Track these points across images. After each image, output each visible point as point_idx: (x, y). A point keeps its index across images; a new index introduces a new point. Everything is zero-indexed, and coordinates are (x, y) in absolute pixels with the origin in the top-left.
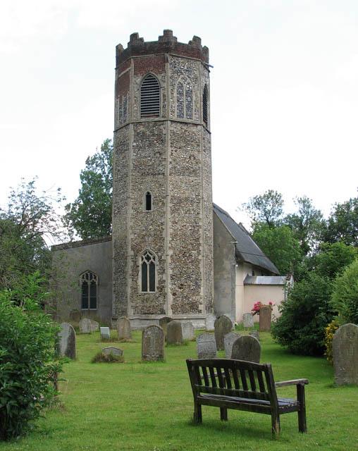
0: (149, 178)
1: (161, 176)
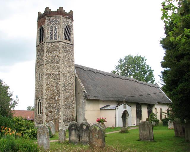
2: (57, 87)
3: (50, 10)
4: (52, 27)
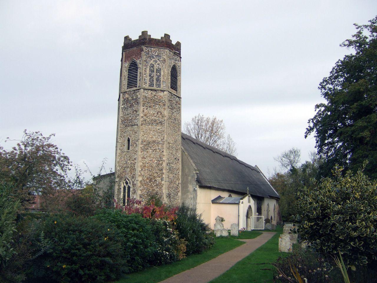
0: (129, 128)
1: (136, 127)
2: (159, 164)
3: (150, 36)
4: (153, 65)
